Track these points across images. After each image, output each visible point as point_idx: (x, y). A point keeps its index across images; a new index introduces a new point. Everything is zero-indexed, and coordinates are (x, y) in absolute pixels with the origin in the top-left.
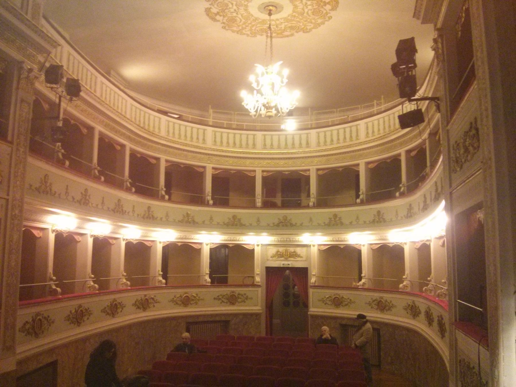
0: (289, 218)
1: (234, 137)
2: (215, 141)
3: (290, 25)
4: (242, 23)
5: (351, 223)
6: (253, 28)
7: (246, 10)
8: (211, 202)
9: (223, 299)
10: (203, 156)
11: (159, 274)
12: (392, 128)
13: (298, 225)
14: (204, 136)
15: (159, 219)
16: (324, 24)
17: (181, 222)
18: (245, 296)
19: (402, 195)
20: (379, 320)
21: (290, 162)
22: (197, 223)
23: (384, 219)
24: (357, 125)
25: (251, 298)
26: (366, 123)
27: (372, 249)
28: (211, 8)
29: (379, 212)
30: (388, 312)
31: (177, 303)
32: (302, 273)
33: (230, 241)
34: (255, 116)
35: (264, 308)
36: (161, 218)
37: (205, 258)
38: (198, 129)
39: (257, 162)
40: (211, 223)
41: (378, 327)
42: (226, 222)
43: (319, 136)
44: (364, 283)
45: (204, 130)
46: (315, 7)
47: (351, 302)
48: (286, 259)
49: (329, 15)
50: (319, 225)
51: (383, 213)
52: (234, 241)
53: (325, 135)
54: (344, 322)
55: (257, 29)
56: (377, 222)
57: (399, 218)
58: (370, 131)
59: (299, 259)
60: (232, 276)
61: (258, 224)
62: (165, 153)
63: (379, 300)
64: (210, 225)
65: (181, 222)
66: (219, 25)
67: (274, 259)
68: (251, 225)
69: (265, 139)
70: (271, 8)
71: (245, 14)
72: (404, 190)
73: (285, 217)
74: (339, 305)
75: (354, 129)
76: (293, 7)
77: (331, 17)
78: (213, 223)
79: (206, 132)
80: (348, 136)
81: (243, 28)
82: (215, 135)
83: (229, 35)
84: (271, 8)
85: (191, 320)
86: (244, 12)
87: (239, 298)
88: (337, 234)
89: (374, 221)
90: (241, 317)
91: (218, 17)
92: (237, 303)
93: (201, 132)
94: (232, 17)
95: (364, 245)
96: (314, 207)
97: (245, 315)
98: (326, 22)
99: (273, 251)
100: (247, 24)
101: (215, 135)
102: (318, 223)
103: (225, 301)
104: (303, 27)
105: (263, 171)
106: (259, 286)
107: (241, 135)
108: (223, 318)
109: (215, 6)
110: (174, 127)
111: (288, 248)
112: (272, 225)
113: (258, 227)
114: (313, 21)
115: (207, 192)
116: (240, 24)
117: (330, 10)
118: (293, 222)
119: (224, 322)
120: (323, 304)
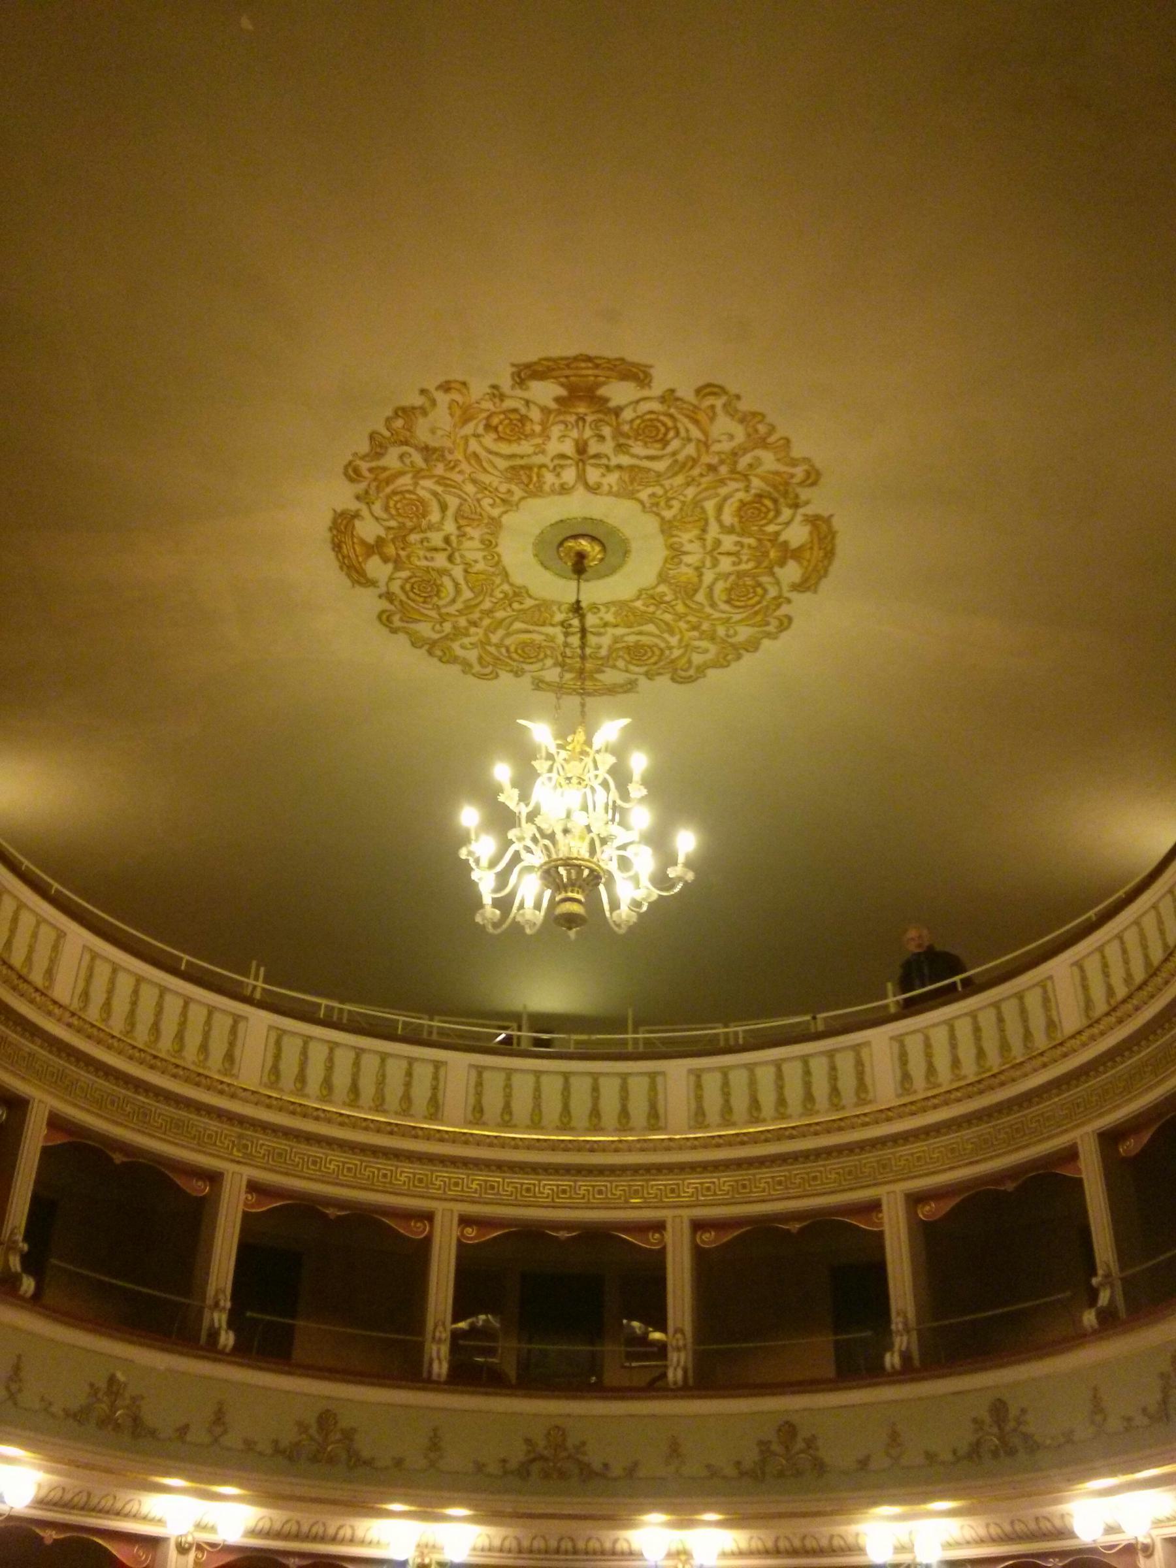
1: (357, 1064)
2: (275, 1070)
3: (632, 639)
4: (459, 605)
5: (864, 1463)
6: (495, 639)
7: (489, 545)
8: (227, 1339)
10: (214, 1125)
14: (232, 1044)
16: (756, 649)
17: (79, 1416)
19: (1109, 1322)
21: (584, 1185)
22: (153, 1433)
23: (1026, 1437)
28: (357, 515)
29: (999, 1409)
33: (297, 1537)
34: (496, 925)
38: (211, 1010)
42: (284, 1444)
45: (237, 1019)
46: (743, 567)
49: (785, 609)
50: (713, 1472)
51: (1023, 1411)
53: (726, 1084)
55: (507, 642)
56: (995, 1454)
57: (1114, 1423)
58: (917, 1068)
61: (432, 1464)
62: (59, 1083)
65: (79, 1416)
66: (369, 602)
68: (399, 1463)
69: (479, 1084)
70: (585, 545)
71: (481, 566)
72: (1112, 1299)
73: (557, 1433)
75: (846, 1063)
76: (666, 553)
77: (790, 619)
78: (227, 1440)
79: (241, 1026)
80: (821, 1088)
81: (458, 633)
83: (398, 656)
84: (585, 545)
86: (479, 555)
88: (804, 1515)
91: (375, 567)
93: (221, 1024)
94: (427, 570)
96: (686, 1390)
98: (766, 643)
100: (475, 616)
104: (676, 653)
105: (465, 1221)
107: (383, 1061)
109: (377, 508)
110: (112, 982)
114: (721, 631)
115: (211, 1290)
116: (452, 610)
117: (795, 587)
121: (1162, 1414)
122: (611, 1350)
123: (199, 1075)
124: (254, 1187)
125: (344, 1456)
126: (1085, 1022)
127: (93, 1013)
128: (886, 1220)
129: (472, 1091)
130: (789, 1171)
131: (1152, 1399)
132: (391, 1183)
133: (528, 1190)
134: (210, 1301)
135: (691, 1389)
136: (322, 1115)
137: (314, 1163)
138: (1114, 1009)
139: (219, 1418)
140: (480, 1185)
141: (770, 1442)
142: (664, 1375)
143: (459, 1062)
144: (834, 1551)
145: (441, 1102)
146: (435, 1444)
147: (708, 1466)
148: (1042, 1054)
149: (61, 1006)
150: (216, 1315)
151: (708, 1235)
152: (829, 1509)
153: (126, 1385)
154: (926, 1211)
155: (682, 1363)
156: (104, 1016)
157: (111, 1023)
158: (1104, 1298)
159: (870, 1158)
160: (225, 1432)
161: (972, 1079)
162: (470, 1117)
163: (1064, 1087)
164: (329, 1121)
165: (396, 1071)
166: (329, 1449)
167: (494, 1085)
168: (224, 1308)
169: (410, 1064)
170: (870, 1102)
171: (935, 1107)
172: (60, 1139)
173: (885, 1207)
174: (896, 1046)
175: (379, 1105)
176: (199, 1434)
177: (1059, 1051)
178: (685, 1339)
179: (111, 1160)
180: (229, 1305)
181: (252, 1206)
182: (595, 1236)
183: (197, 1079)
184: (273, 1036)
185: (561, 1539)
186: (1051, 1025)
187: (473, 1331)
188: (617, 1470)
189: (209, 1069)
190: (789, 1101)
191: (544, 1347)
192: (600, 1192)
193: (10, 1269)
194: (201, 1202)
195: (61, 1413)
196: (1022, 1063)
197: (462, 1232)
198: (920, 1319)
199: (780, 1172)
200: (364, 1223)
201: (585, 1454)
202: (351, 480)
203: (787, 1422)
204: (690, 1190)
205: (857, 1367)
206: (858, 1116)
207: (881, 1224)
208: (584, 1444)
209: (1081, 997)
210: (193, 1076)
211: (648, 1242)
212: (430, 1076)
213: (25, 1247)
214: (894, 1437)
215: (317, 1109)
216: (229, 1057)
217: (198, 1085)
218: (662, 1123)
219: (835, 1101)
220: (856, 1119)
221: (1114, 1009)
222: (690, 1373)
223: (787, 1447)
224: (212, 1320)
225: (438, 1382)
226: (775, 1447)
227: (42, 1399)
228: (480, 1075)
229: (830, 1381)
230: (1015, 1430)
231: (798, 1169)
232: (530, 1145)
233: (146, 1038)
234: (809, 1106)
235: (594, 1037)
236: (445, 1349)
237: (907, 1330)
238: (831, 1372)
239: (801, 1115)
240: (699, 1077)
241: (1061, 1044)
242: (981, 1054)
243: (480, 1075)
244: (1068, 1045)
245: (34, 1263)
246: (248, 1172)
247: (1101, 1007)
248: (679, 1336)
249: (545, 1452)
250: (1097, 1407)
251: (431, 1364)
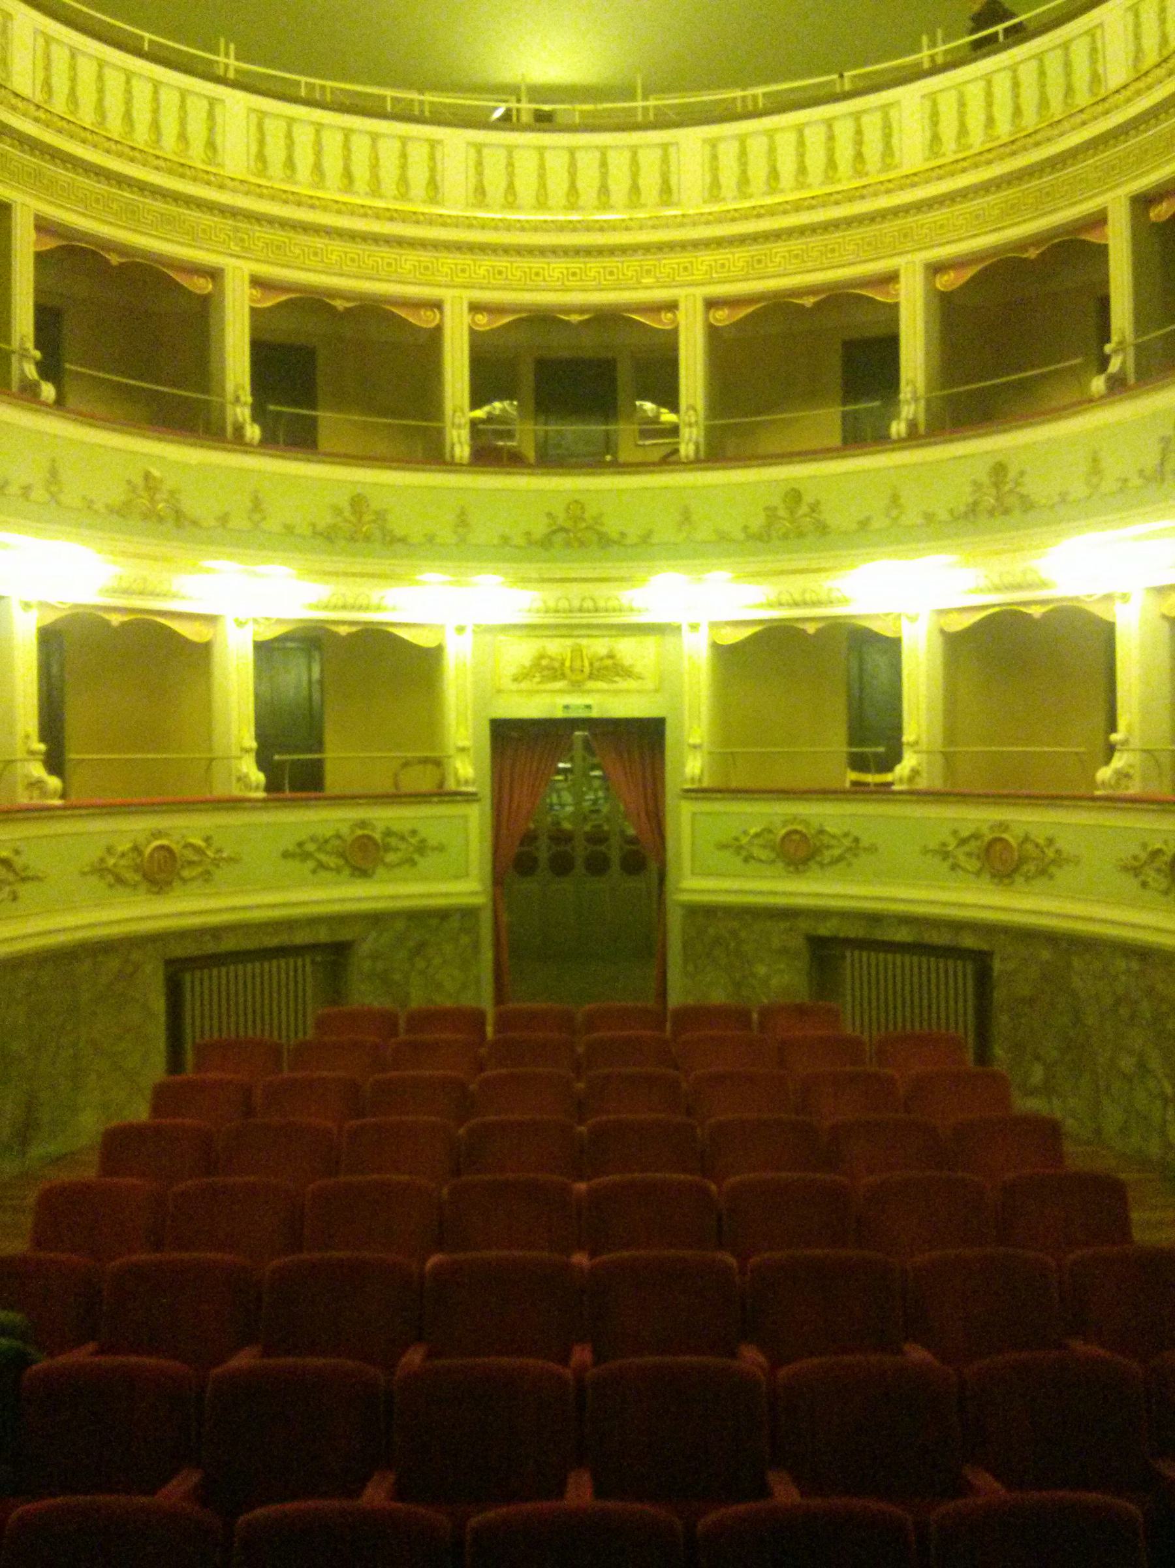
0: (591, 511)
1: (347, 146)
2: (261, 157)
5: (864, 524)
8: (253, 432)
9: (322, 857)
10: (208, 220)
11: (32, 753)
12: (1057, 109)
13: (628, 541)
14: (211, 130)
15: (13, 489)
18: (413, 841)
19: (1118, 387)
20: (921, 910)
21: (594, 266)
22: (195, 523)
23: (1022, 497)
24: (885, 108)
25: (441, 848)
26: (932, 97)
27: (942, 632)
29: (999, 470)
30: (1039, 883)
31: (120, 880)
32: (638, 743)
35: (489, 882)
36: (26, 490)
37: (233, 677)
39: (448, 262)
40: (256, 525)
41: (985, 947)
43: (714, 157)
44: (915, 773)
45: (212, 102)
47: (855, 847)
48: (576, 687)
50: (722, 537)
51: (1022, 473)
52: (360, 608)
53: (743, 153)
54: (824, 930)
57: (1109, 484)
58: (948, 129)
59: (631, 684)
60: (340, 760)
61: (462, 540)
63: (989, 837)
64: (249, 529)
67: (525, 685)
68: (430, 539)
69: (479, 164)
72: (1122, 368)
74: (806, 861)
75: (872, 126)
78: (265, 526)
79: (218, 109)
82: (260, 127)
85: (179, 951)
87: (387, 848)
89: (973, 510)
90: (400, 925)
92: (381, 871)
95: (912, 619)
97: (418, 918)
99: (520, 652)
101: (260, 127)
102: (717, 531)
103: (332, 861)
105: (475, 308)
106: (470, 798)
108: (323, 935)
111: (584, 642)
112: (520, 540)
113: (459, 544)
115: (230, 387)
118: (612, 527)
119: (327, 951)
120: (738, 861)
121: (1158, 476)
122: (625, 430)
123: (183, 165)
124: (257, 282)
125: (378, 534)
126: (1134, 75)
127: (59, 105)
128: (902, 292)
129: (472, 171)
130: (807, 244)
131: (1151, 460)
132: (396, 271)
133: (537, 274)
134: (230, 396)
135: (704, 461)
136: (317, 203)
137: (316, 254)
138: (1165, 60)
139: (257, 505)
140: (488, 271)
141: (776, 508)
142: (676, 451)
143: (455, 140)
144: (831, 602)
145: (439, 184)
146: (463, 521)
148: (1081, 111)
149: (23, 99)
150: (238, 410)
151: (720, 313)
152: (827, 565)
153: (161, 481)
154: (945, 282)
155: (694, 436)
156: (72, 107)
157: (81, 114)
158: (1114, 365)
159: (890, 227)
160: (264, 518)
161: (1005, 139)
162: (472, 200)
163: (1101, 147)
164: (325, 209)
165: (389, 152)
166: (364, 529)
167: (495, 163)
168: (245, 404)
169: (404, 145)
170: (896, 167)
171: (964, 170)
172: (51, 244)
173: (902, 279)
174: (928, 104)
175: (375, 190)
176: (239, 521)
177: (1100, 108)
178: (697, 415)
179: (107, 262)
180: (249, 399)
181: (259, 301)
182: (608, 319)
183: (181, 170)
184: (254, 119)
185: (583, 599)
186: (1096, 79)
187: (490, 419)
188: (632, 539)
189: (191, 158)
190: (810, 169)
191: (559, 428)
192: (611, 273)
193: (26, 377)
194: (205, 300)
195: (103, 510)
196: (1059, 122)
197: (473, 319)
198: (929, 387)
199: (796, 245)
200: (372, 313)
201: (602, 524)
203: (793, 489)
204: (704, 268)
205: (861, 436)
206: (881, 183)
207: (897, 295)
208: (601, 515)
209: (1132, 47)
210: (175, 167)
211: (660, 322)
212: (426, 156)
213: (38, 354)
214: (895, 500)
215: (311, 197)
216: (211, 145)
217: (182, 176)
218: (675, 197)
219: (859, 167)
220: (879, 186)
221: (1165, 60)
222: (702, 448)
223: (792, 513)
224: (235, 414)
225: (462, 465)
226: (782, 512)
227: (84, 498)
228: (479, 152)
229: (836, 449)
230: (1011, 491)
231: (816, 241)
232: (537, 228)
233: (146, 137)
234: (831, 174)
235: (600, 107)
236: (465, 434)
237: (916, 399)
238: (837, 441)
239: (823, 184)
240: (714, 146)
241: (1103, 100)
242: (1017, 112)
243: (479, 152)
244: (1111, 100)
245: (50, 369)
246: (250, 267)
247: (1151, 58)
248: (691, 412)
250: (1096, 467)
251: (452, 448)
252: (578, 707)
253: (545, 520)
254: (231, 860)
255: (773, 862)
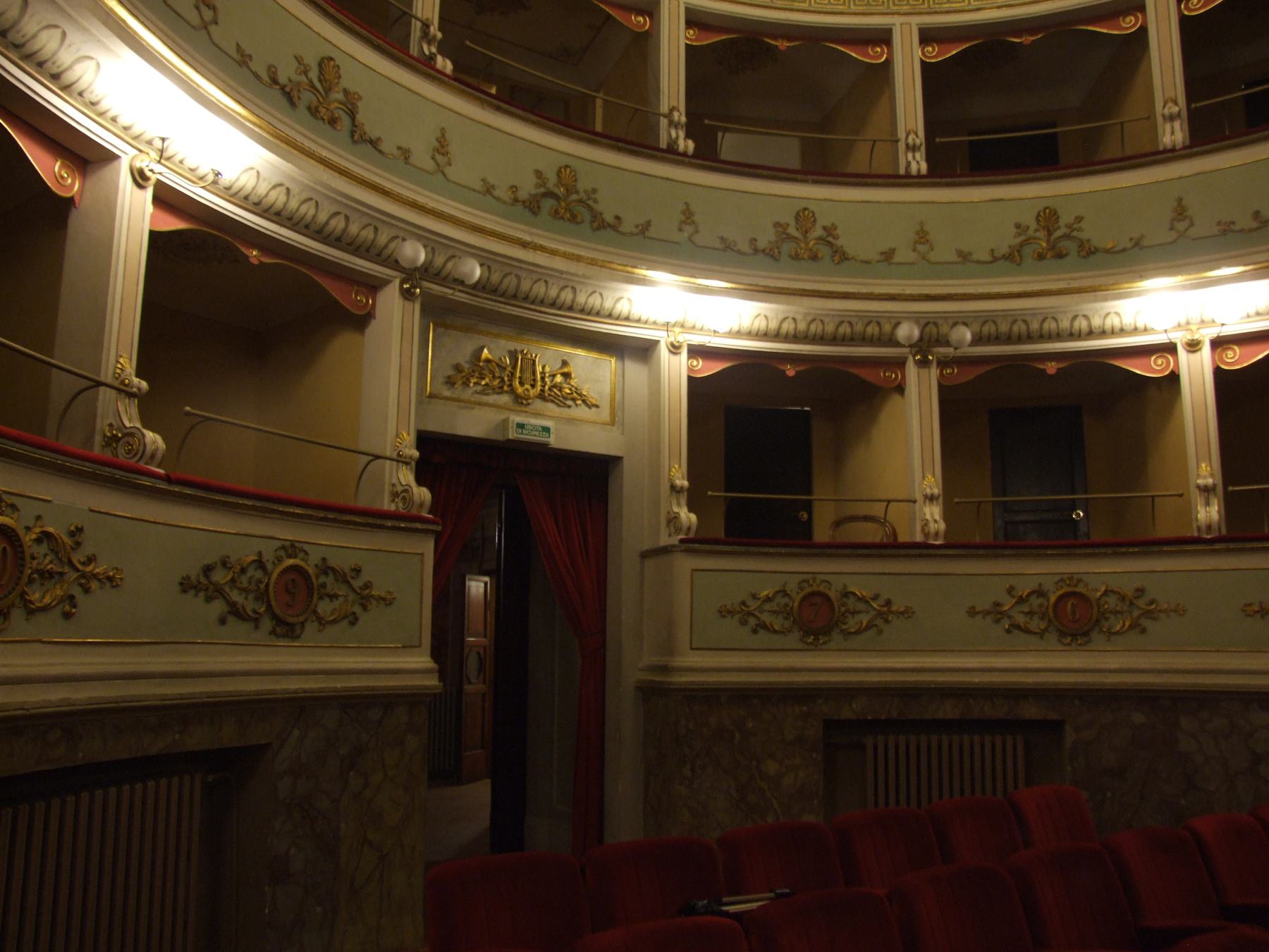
9: (236, 596)
41: (1053, 716)
47: (886, 612)
59: (581, 412)
74: (827, 631)
78: (1193, 232)
112: (505, 195)
119: (1028, 723)
147: (722, 238)
188: (627, 227)
202: (357, 619)
230: (1067, 237)
249: (556, 190)
252: (534, 427)
253: (533, 180)
254: (110, 580)
255: (790, 631)
